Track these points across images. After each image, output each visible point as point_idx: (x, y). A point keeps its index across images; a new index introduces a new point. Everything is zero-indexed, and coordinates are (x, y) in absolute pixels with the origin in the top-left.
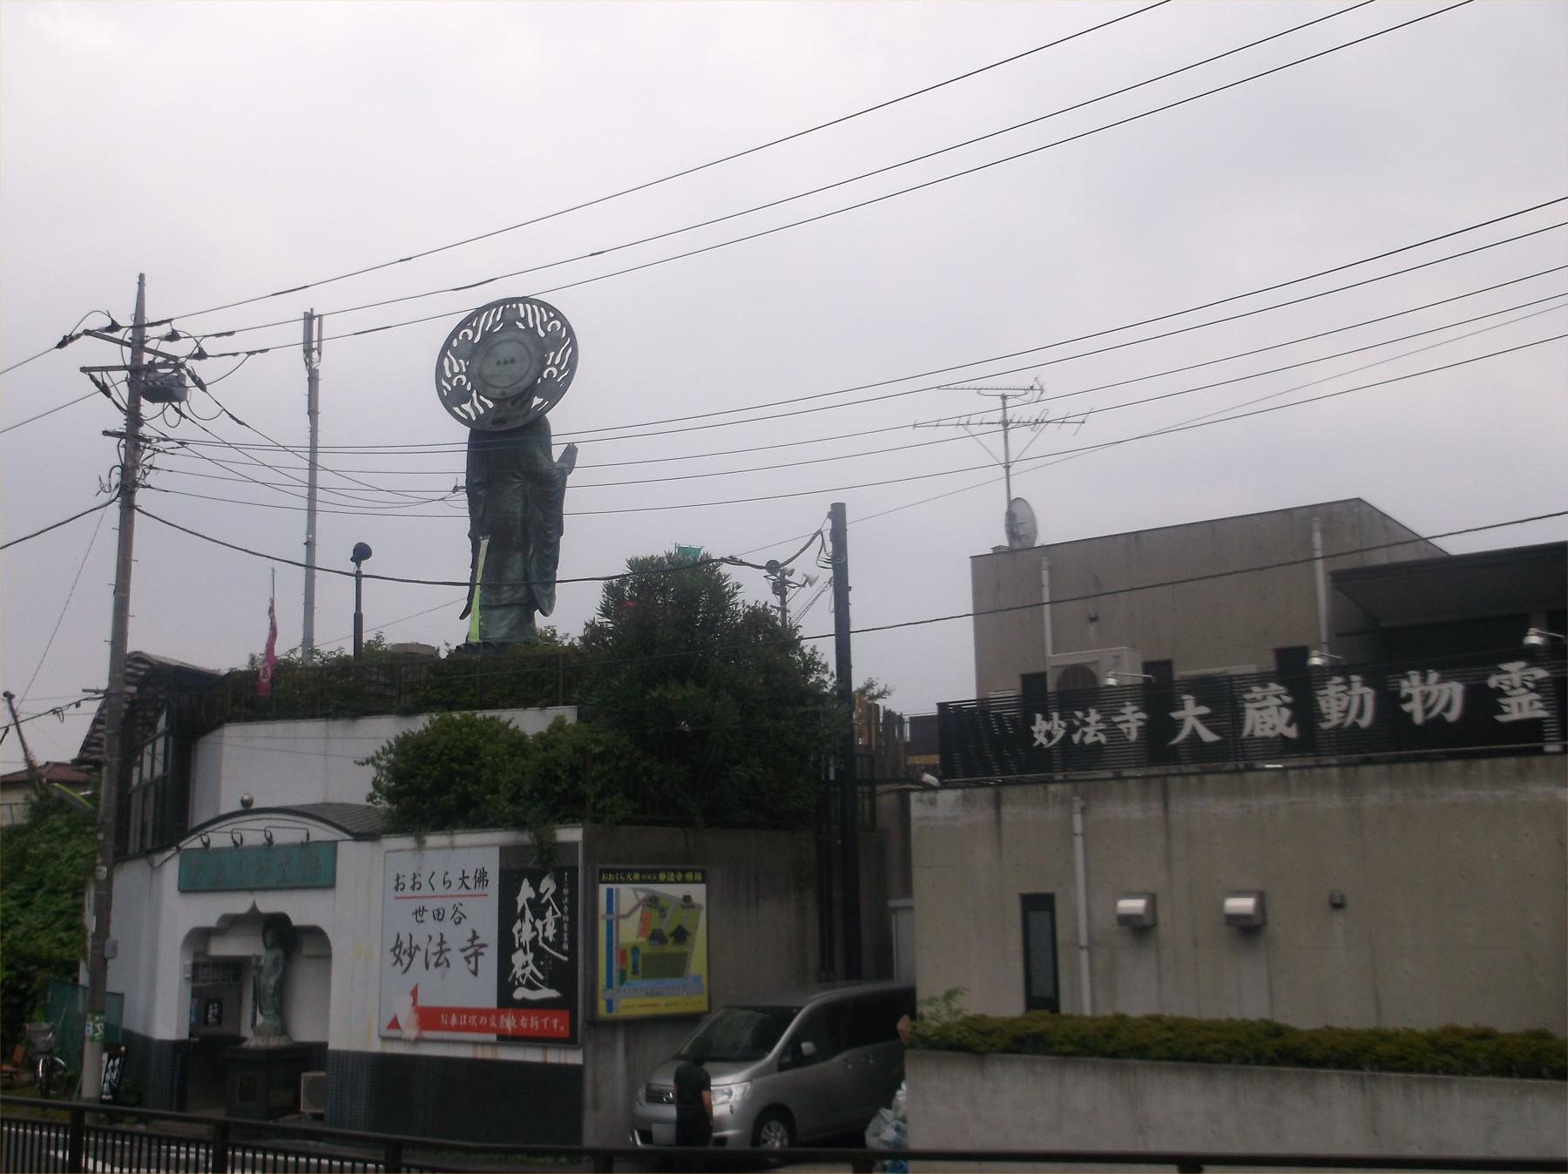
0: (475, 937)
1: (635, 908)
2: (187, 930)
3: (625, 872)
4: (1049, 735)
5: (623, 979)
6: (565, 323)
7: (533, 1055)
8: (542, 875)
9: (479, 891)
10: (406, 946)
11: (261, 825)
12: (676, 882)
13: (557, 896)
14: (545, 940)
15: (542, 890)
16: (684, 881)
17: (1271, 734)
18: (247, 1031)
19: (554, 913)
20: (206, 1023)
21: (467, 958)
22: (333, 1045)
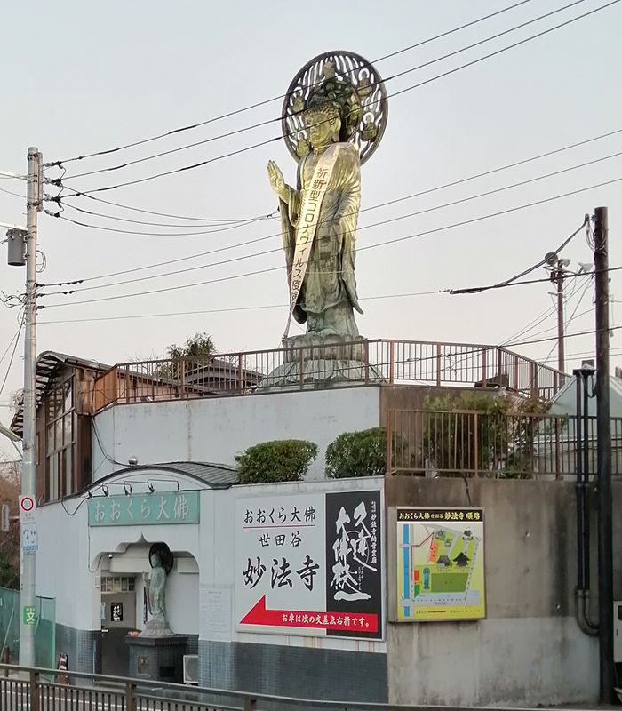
0: (309, 561)
2: (97, 554)
5: (417, 592)
9: (309, 522)
11: (145, 478)
12: (459, 520)
13: (367, 521)
14: (359, 555)
15: (355, 517)
16: (465, 519)
18: (140, 625)
19: (365, 534)
20: (113, 620)
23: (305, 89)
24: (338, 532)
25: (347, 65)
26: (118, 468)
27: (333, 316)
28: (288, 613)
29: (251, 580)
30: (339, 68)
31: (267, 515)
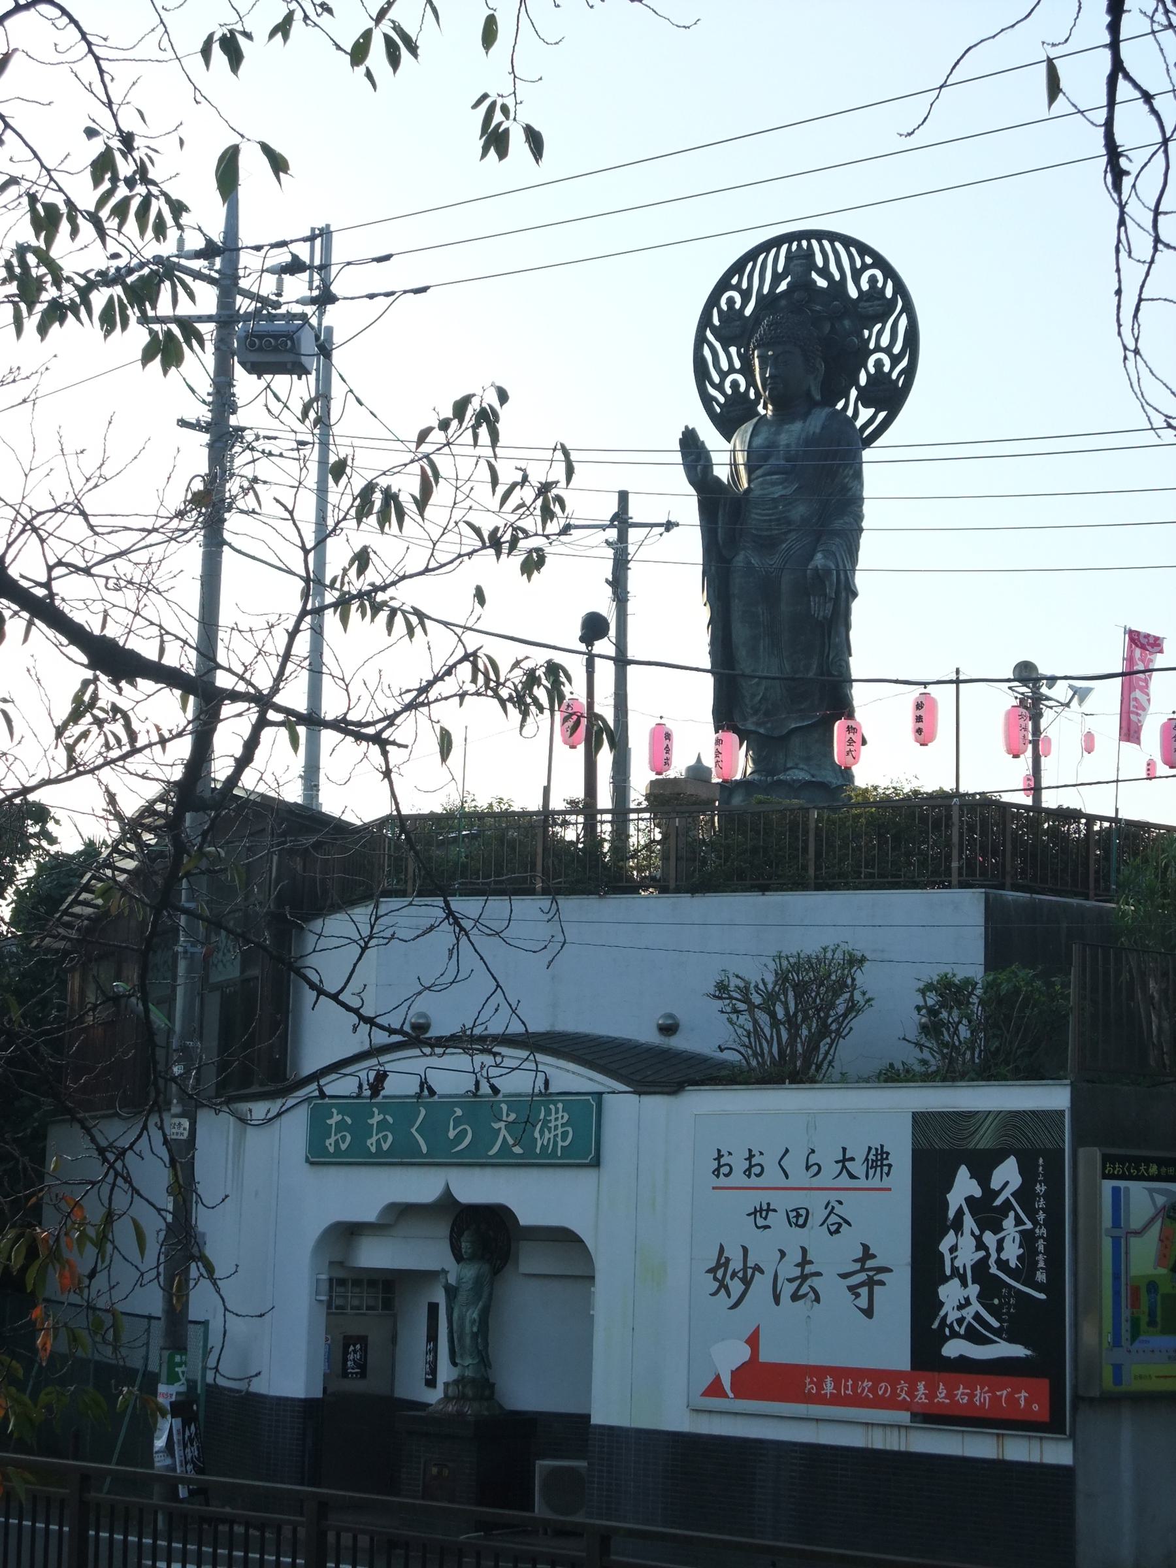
0: (867, 1254)
1: (1152, 1220)
3: (1137, 1161)
5: (1135, 1334)
6: (889, 272)
7: (980, 1447)
8: (998, 1157)
9: (875, 1182)
10: (736, 1264)
13: (1024, 1195)
14: (1002, 1265)
15: (995, 1184)
19: (1019, 1222)
20: (345, 1374)
21: (851, 1289)
22: (596, 1419)
23: (746, 295)
24: (951, 1214)
30: (819, 262)
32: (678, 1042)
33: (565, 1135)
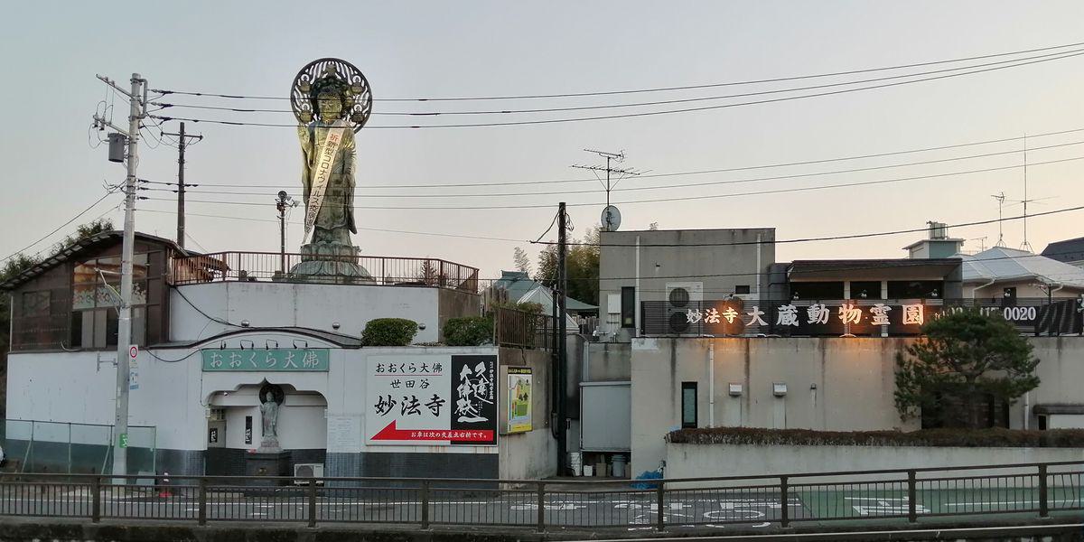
4: (694, 318)
6: (363, 78)
13: (486, 374)
17: (789, 324)
19: (484, 381)
23: (311, 77)
25: (346, 71)
26: (231, 329)
27: (339, 233)
28: (417, 431)
29: (381, 410)
31: (398, 368)
32: (339, 331)
33: (315, 362)
